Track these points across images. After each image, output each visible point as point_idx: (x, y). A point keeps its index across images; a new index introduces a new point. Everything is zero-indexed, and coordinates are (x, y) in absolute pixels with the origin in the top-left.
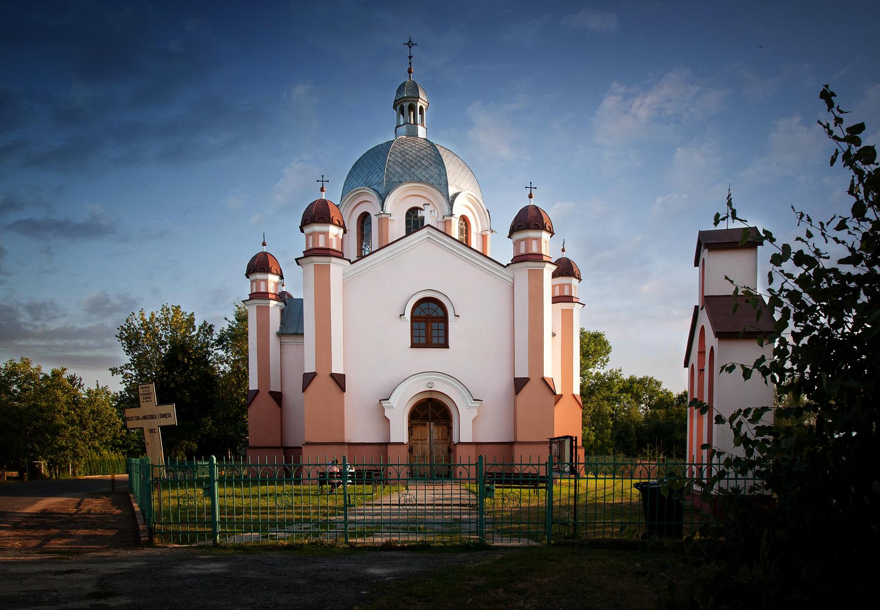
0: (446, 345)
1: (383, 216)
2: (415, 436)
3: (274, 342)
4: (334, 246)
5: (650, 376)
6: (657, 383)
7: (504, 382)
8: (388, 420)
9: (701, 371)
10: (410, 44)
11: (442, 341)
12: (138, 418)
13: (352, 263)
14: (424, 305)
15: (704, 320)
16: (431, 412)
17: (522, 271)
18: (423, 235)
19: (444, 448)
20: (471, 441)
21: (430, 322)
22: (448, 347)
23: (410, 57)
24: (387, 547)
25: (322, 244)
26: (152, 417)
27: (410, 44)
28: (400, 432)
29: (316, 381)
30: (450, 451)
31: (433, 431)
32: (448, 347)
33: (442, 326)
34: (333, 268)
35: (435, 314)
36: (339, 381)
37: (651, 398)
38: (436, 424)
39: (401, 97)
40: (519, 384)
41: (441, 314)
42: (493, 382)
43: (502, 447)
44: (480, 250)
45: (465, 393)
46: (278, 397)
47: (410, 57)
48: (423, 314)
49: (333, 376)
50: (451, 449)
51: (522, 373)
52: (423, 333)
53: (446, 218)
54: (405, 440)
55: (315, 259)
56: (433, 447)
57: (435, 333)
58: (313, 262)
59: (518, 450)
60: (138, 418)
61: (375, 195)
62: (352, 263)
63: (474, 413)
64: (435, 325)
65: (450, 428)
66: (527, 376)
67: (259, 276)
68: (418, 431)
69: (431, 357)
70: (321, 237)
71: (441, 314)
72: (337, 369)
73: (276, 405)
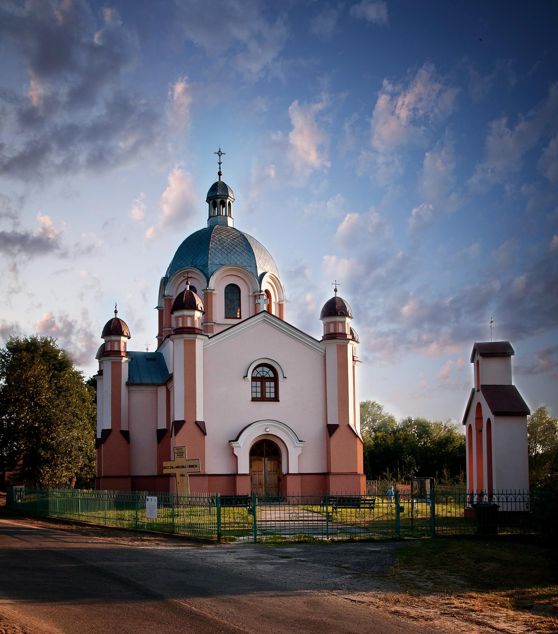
1: (209, 291)
2: (255, 468)
3: (124, 389)
4: (197, 326)
5: (372, 400)
6: (379, 407)
8: (236, 457)
9: (480, 431)
11: (273, 396)
12: (172, 468)
13: (209, 338)
14: (260, 369)
15: (480, 398)
16: (267, 449)
17: (332, 347)
18: (259, 319)
19: (275, 477)
21: (266, 381)
22: (278, 401)
23: (220, 163)
25: (189, 325)
26: (183, 467)
28: (244, 467)
29: (185, 426)
30: (279, 480)
31: (267, 465)
32: (278, 401)
34: (197, 342)
35: (267, 376)
36: (201, 427)
37: (374, 421)
38: (269, 460)
39: (214, 195)
40: (331, 429)
41: (272, 375)
42: (312, 427)
43: (317, 476)
44: (277, 316)
45: (292, 436)
46: (126, 435)
47: (220, 163)
48: (259, 375)
49: (196, 423)
50: (282, 478)
51: (333, 421)
52: (259, 390)
53: (256, 294)
54: (247, 471)
55: (185, 336)
56: (267, 477)
57: (267, 390)
58: (183, 338)
59: (333, 480)
60: (172, 468)
61: (198, 272)
62: (209, 338)
63: (299, 451)
64: (267, 384)
67: (114, 338)
68: (256, 464)
70: (189, 319)
71: (272, 375)
72: (199, 418)
73: (126, 442)
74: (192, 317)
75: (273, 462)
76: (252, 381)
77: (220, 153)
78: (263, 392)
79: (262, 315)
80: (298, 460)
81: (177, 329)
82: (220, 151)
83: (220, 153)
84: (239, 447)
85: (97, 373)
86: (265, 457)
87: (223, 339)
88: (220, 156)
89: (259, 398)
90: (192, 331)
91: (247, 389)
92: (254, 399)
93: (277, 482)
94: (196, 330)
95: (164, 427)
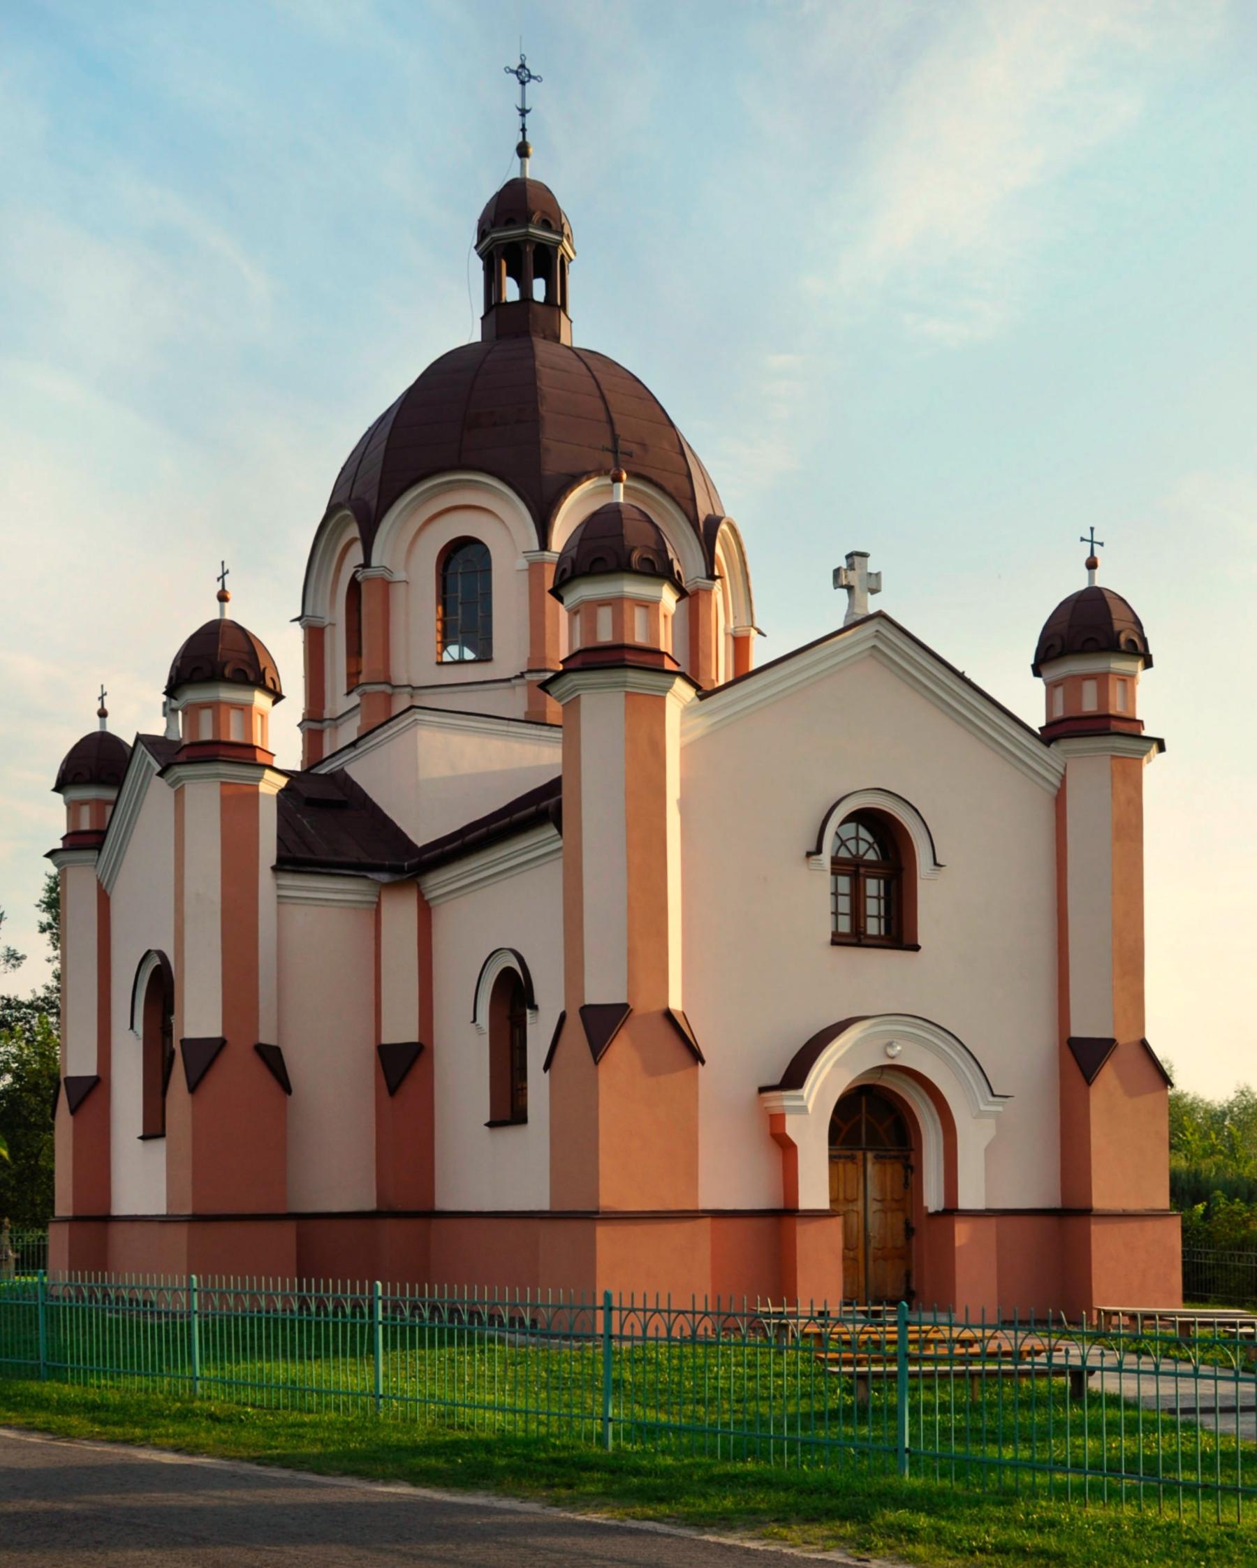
4: (665, 645)
21: (879, 873)
22: (916, 948)
30: (909, 1231)
31: (875, 1175)
42: (1018, 1048)
46: (271, 1058)
47: (523, 112)
55: (223, 769)
74: (650, 605)
75: (889, 1169)
76: (835, 873)
77: (523, 75)
78: (857, 914)
79: (870, 628)
80: (987, 1162)
81: (192, 745)
82: (522, 66)
83: (523, 75)
84: (803, 1110)
85: (59, 845)
86: (865, 1150)
87: (738, 708)
88: (523, 83)
89: (843, 935)
90: (648, 660)
91: (815, 896)
92: (838, 940)
93: (900, 1242)
94: (259, 753)
95: (91, 1070)
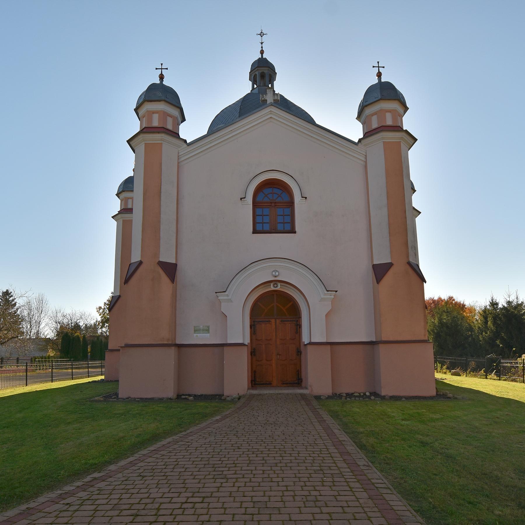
0: (293, 231)
7: (362, 268)
10: (262, 34)
14: (267, 191)
16: (276, 308)
20: (324, 340)
22: (295, 232)
23: (262, 43)
24: (37, 495)
27: (262, 34)
28: (239, 332)
32: (295, 232)
33: (287, 211)
36: (170, 270)
43: (361, 347)
47: (262, 43)
48: (266, 200)
54: (247, 341)
65: (299, 326)
66: (389, 261)
69: (275, 243)
